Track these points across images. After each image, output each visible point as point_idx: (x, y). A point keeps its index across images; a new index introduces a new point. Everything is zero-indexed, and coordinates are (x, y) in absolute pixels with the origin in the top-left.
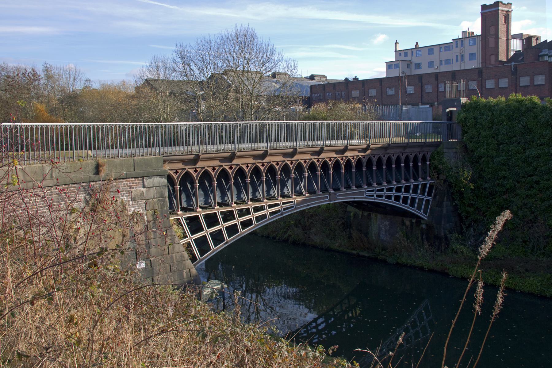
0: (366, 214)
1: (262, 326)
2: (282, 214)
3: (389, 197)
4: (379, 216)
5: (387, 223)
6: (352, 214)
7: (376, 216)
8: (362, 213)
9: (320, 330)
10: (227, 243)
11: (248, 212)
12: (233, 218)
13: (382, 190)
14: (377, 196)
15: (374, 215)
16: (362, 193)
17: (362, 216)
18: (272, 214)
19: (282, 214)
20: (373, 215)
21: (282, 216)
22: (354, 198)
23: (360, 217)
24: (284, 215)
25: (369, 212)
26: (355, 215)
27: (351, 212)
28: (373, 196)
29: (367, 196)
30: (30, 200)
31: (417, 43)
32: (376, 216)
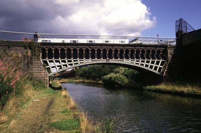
3: (143, 65)
11: (71, 61)
13: (139, 61)
14: (136, 63)
16: (123, 61)
18: (80, 63)
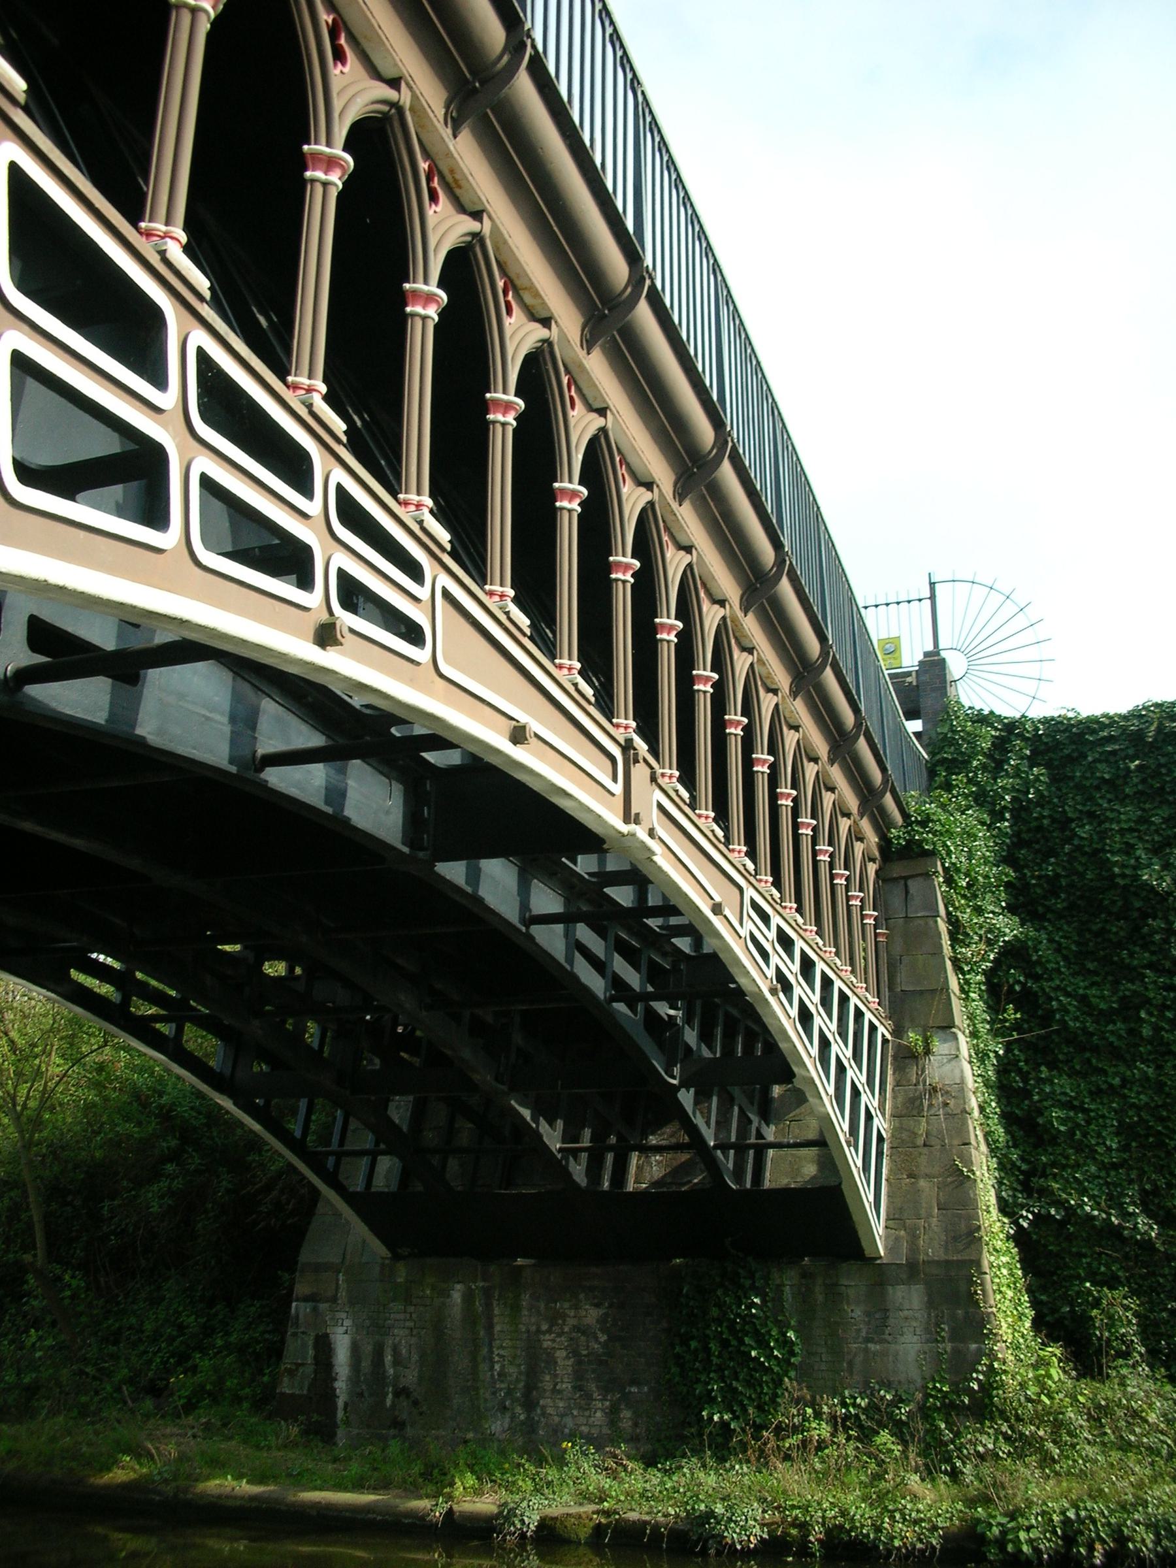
5: (591, 1315)
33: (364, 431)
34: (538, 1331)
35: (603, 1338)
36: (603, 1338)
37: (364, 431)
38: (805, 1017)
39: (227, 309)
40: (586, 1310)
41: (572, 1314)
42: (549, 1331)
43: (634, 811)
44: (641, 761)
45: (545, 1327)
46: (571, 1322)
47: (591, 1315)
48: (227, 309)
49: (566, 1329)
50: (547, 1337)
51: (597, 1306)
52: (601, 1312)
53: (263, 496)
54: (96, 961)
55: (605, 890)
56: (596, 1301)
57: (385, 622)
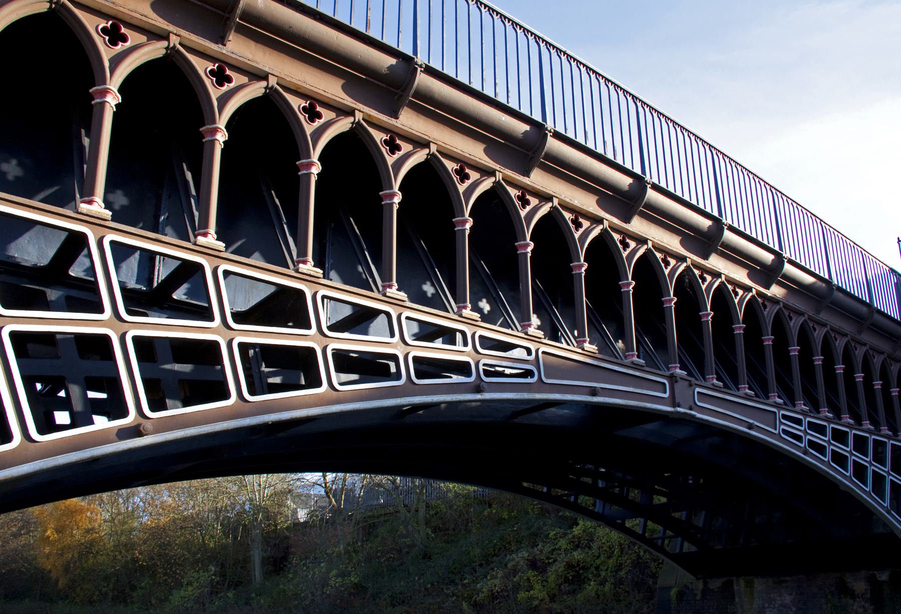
0: (716, 584)
1: (217, 511)
2: (478, 388)
4: (759, 584)
5: (787, 599)
6: (673, 592)
7: (750, 585)
8: (705, 584)
9: (541, 323)
10: (135, 431)
12: (466, 373)
15: (742, 583)
17: (704, 592)
19: (478, 388)
20: (740, 585)
21: (478, 396)
22: (751, 427)
23: (699, 597)
24: (487, 396)
25: (726, 579)
26: (681, 594)
27: (670, 588)
28: (798, 438)
29: (784, 431)
30: (314, 499)
31: (898, 238)
32: (750, 585)
33: (435, 266)
34: (764, 607)
35: (794, 609)
36: (794, 609)
37: (435, 266)
38: (860, 471)
39: (433, 262)
40: (785, 597)
41: (779, 599)
42: (769, 607)
43: (677, 401)
44: (694, 385)
45: (766, 605)
46: (779, 602)
47: (787, 599)
48: (433, 262)
49: (777, 606)
50: (768, 609)
51: (790, 594)
52: (792, 597)
53: (189, 254)
54: (666, 489)
55: (38, 390)
56: (789, 592)
57: (370, 319)
